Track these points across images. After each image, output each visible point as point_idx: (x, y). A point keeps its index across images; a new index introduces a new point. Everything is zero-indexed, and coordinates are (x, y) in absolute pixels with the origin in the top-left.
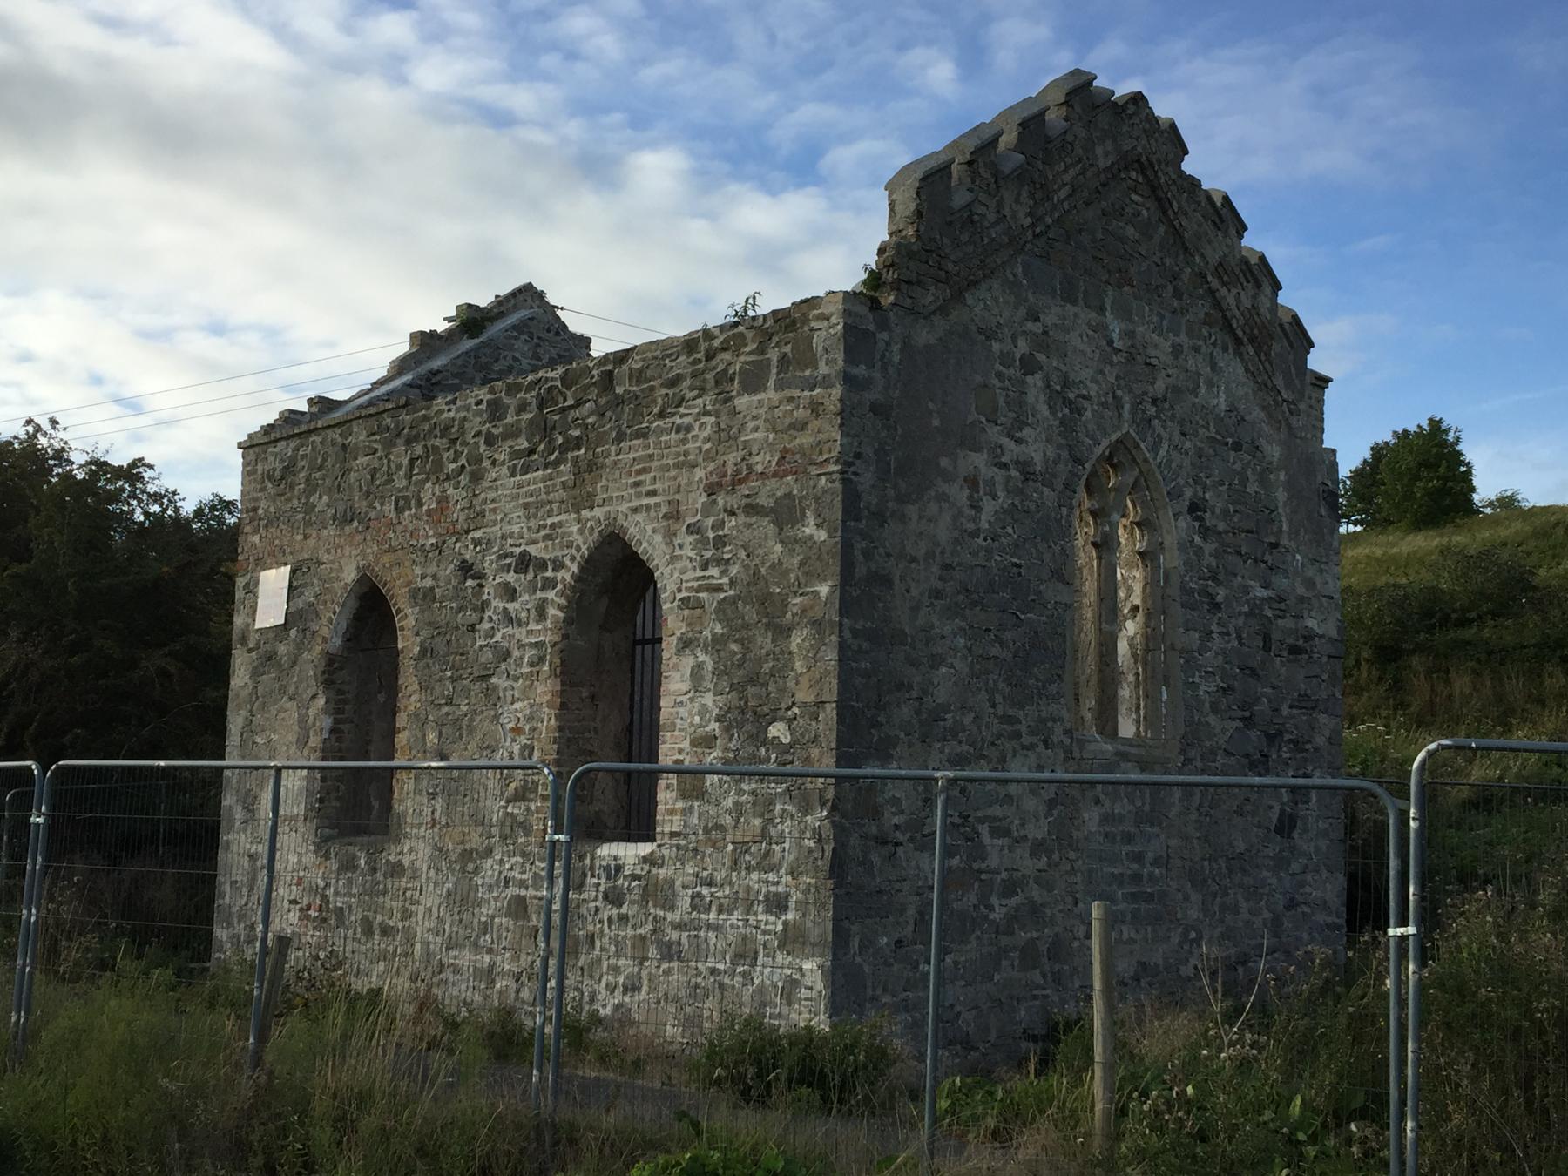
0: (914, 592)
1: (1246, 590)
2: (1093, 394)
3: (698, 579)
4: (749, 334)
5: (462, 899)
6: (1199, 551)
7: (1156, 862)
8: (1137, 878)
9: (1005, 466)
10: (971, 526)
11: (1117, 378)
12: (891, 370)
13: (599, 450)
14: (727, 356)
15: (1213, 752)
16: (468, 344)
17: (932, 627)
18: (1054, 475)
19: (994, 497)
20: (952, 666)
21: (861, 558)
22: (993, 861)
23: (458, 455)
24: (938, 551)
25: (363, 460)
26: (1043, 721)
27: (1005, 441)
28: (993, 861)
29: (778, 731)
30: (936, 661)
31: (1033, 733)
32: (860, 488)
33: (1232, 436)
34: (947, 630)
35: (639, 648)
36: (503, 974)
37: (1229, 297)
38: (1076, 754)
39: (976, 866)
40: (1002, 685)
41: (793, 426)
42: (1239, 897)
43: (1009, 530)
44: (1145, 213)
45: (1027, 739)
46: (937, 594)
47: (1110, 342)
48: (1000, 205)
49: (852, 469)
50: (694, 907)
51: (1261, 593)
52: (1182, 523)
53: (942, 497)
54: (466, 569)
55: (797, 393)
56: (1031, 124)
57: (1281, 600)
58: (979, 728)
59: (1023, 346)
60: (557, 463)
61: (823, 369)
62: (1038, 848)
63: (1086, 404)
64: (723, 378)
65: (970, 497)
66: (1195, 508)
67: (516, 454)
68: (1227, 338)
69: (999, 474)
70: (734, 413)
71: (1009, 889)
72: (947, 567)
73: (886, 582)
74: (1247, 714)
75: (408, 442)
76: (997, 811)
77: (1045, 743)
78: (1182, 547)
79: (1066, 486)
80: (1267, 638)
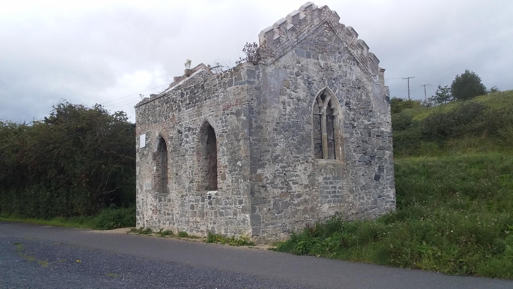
0: (269, 130)
1: (363, 122)
4: (229, 73)
5: (182, 205)
6: (349, 114)
10: (284, 113)
11: (323, 75)
12: (260, 79)
14: (225, 79)
15: (355, 162)
16: (187, 78)
18: (306, 99)
22: (294, 190)
23: (176, 106)
25: (158, 108)
28: (294, 190)
29: (239, 163)
30: (276, 145)
34: (279, 138)
36: (191, 222)
37: (354, 52)
44: (329, 34)
45: (301, 162)
46: (275, 130)
47: (321, 67)
48: (287, 37)
50: (226, 204)
51: (367, 122)
52: (343, 108)
54: (180, 132)
55: (238, 86)
56: (295, 17)
57: (374, 124)
59: (296, 70)
60: (194, 106)
61: (243, 80)
62: (306, 186)
63: (314, 82)
64: (225, 84)
67: (187, 105)
68: (355, 62)
70: (227, 92)
71: (299, 196)
72: (278, 123)
73: (261, 127)
75: (166, 104)
76: (294, 178)
77: (307, 162)
78: (344, 114)
80: (370, 133)
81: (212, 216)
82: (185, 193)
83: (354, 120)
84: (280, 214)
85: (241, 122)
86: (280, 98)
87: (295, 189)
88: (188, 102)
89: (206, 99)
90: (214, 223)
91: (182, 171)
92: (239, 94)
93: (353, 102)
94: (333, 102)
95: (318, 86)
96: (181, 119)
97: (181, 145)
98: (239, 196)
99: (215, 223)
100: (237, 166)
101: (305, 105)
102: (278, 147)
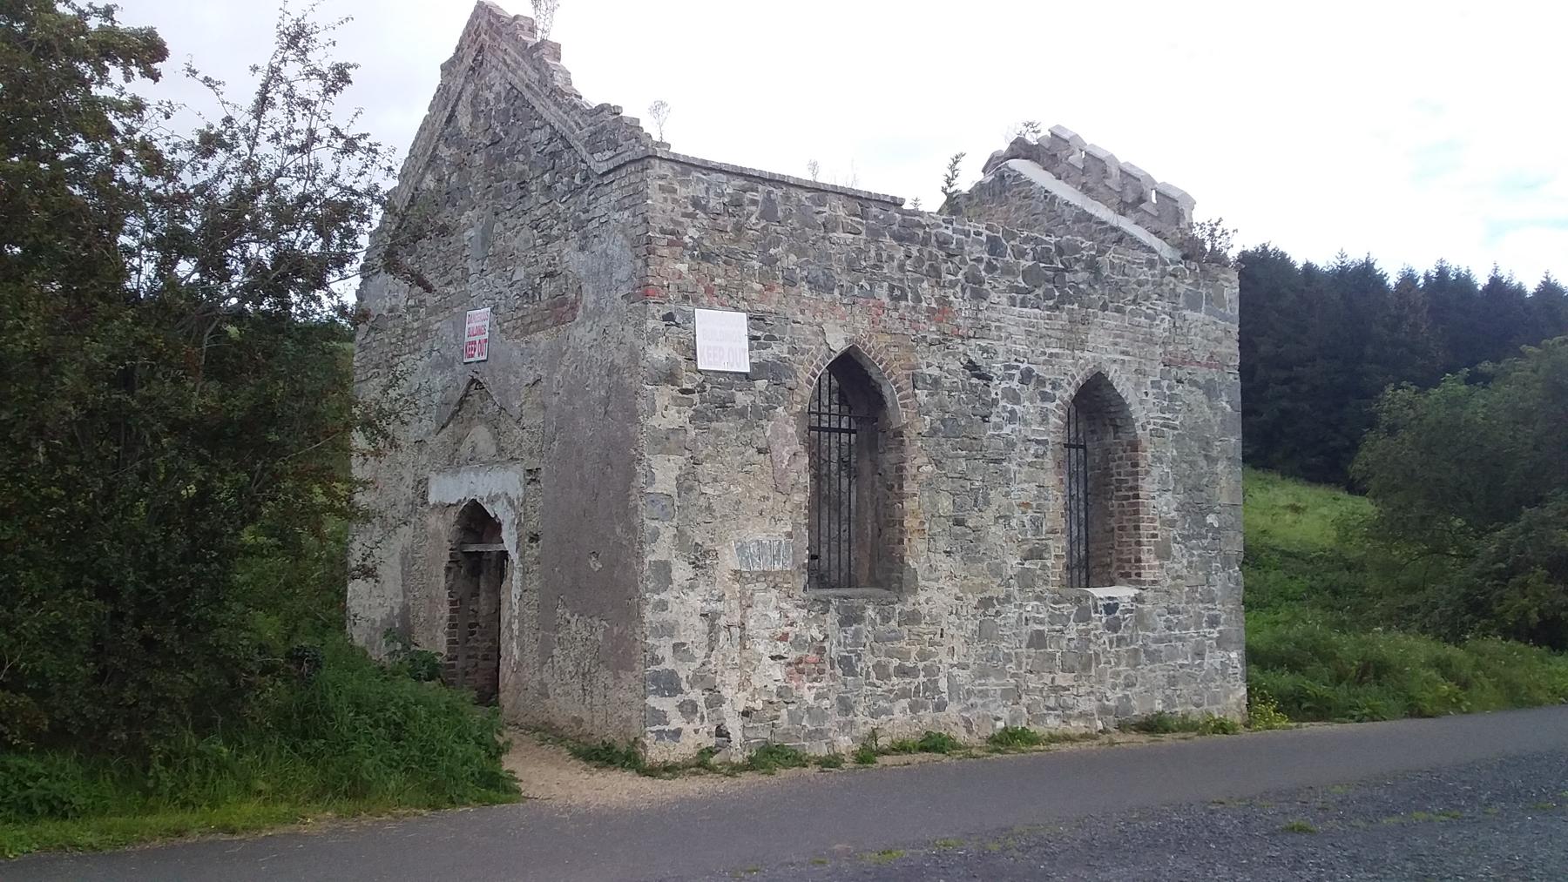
82: (996, 591)
90: (1129, 685)
91: (990, 514)
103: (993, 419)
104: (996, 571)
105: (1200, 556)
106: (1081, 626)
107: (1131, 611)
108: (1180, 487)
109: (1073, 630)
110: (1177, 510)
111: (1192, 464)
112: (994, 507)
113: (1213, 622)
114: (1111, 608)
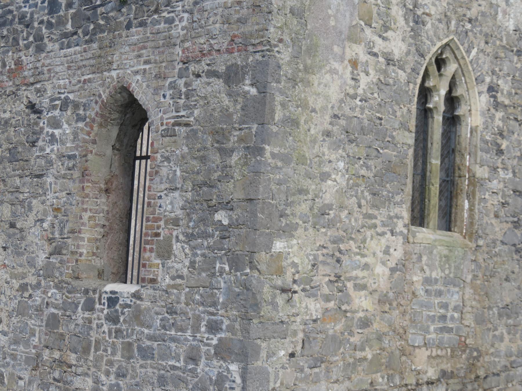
0: (312, 132)
2: (433, 13)
3: (174, 117)
6: (492, 118)
7: (455, 309)
8: (443, 318)
9: (375, 55)
10: (351, 92)
13: (117, 33)
17: (324, 155)
18: (406, 62)
19: (367, 74)
20: (335, 181)
21: (279, 107)
23: (29, 34)
24: (330, 106)
26: (390, 218)
27: (376, 38)
30: (325, 177)
31: (384, 225)
32: (281, 62)
33: (516, 46)
34: (333, 157)
35: (137, 162)
38: (411, 240)
39: (343, 308)
40: (366, 194)
41: (239, 20)
42: (504, 331)
43: (376, 95)
45: (380, 230)
46: (328, 134)
49: (276, 49)
50: (164, 327)
53: (333, 72)
54: (32, 107)
58: (350, 221)
60: (90, 41)
63: (427, 19)
65: (352, 73)
66: (492, 89)
69: (371, 59)
72: (336, 116)
73: (295, 123)
74: (516, 219)
76: (360, 273)
79: (413, 70)
81: (114, 354)
82: (32, 280)
83: (501, 134)
84: (317, 370)
85: (240, 100)
86: (348, 50)
87: (362, 303)
88: (69, 27)
89: (129, 26)
90: (120, 375)
91: (32, 217)
92: (242, 21)
93: (504, 85)
94: (461, 80)
95: (435, 33)
96: (41, 73)
97: (33, 144)
98: (212, 309)
99: (124, 376)
100: (214, 223)
101: (402, 76)
102: (329, 182)
103: (40, 143)
104: (31, 263)
105: (203, 255)
106: (87, 315)
107: (129, 306)
108: (189, 185)
109: (81, 315)
110: (183, 208)
111: (203, 159)
112: (34, 212)
113: (214, 328)
114: (113, 301)
